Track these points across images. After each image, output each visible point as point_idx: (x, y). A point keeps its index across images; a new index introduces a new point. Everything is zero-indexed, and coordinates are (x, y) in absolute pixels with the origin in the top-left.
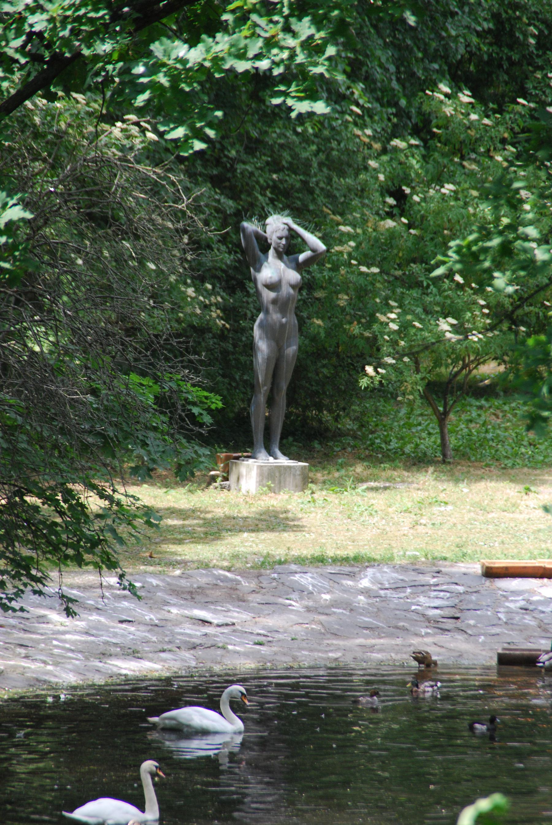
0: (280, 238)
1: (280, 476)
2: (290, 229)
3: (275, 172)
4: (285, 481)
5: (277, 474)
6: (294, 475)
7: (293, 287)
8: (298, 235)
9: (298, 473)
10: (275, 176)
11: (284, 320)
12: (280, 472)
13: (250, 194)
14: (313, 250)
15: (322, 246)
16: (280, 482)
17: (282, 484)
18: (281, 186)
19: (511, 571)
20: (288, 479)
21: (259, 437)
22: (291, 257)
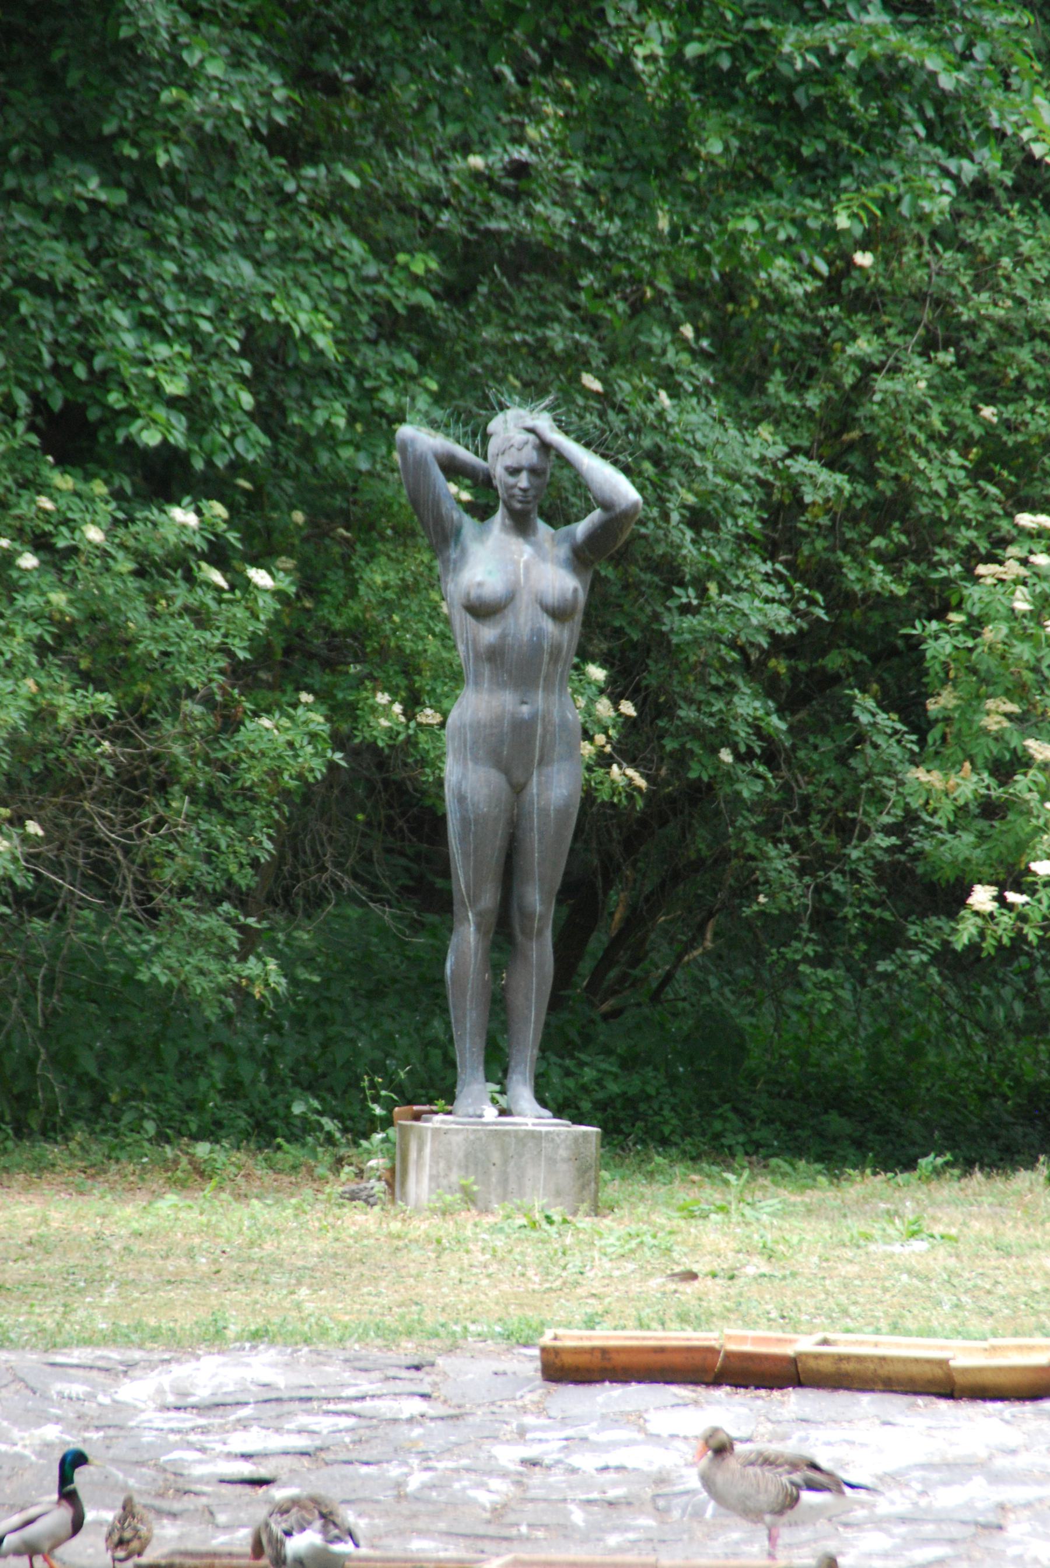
0: (514, 471)
1: (505, 1162)
2: (545, 447)
3: (991, 400)
4: (520, 1178)
5: (496, 1156)
6: (551, 1161)
7: (558, 613)
8: (564, 461)
9: (563, 1153)
10: (988, 412)
11: (525, 709)
12: (503, 1149)
13: (900, 458)
14: (607, 506)
15: (625, 491)
16: (504, 1181)
17: (513, 1186)
18: (1010, 440)
19: (621, 1360)
20: (530, 1172)
21: (469, 1052)
22: (564, 529)
